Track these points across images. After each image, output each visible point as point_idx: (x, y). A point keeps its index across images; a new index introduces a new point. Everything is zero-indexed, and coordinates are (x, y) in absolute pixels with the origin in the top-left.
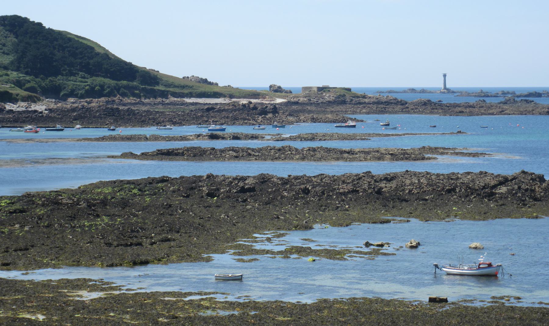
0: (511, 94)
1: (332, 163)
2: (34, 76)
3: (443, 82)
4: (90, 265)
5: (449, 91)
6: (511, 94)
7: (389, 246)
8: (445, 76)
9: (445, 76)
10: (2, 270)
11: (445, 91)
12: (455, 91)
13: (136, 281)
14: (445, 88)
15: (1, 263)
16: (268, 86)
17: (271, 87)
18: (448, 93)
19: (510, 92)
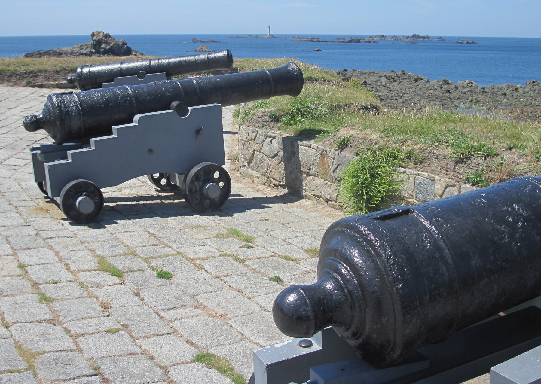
0: (317, 39)
1: (193, 58)
2: (300, 169)
3: (269, 31)
4: (217, 68)
5: (272, 36)
6: (317, 39)
7: (346, 70)
8: (270, 27)
9: (270, 27)
10: (2, 85)
11: (270, 36)
12: (276, 36)
13: (194, 78)
14: (270, 35)
15: (133, 49)
16: (90, 34)
17: (93, 35)
18: (272, 37)
19: (316, 38)
